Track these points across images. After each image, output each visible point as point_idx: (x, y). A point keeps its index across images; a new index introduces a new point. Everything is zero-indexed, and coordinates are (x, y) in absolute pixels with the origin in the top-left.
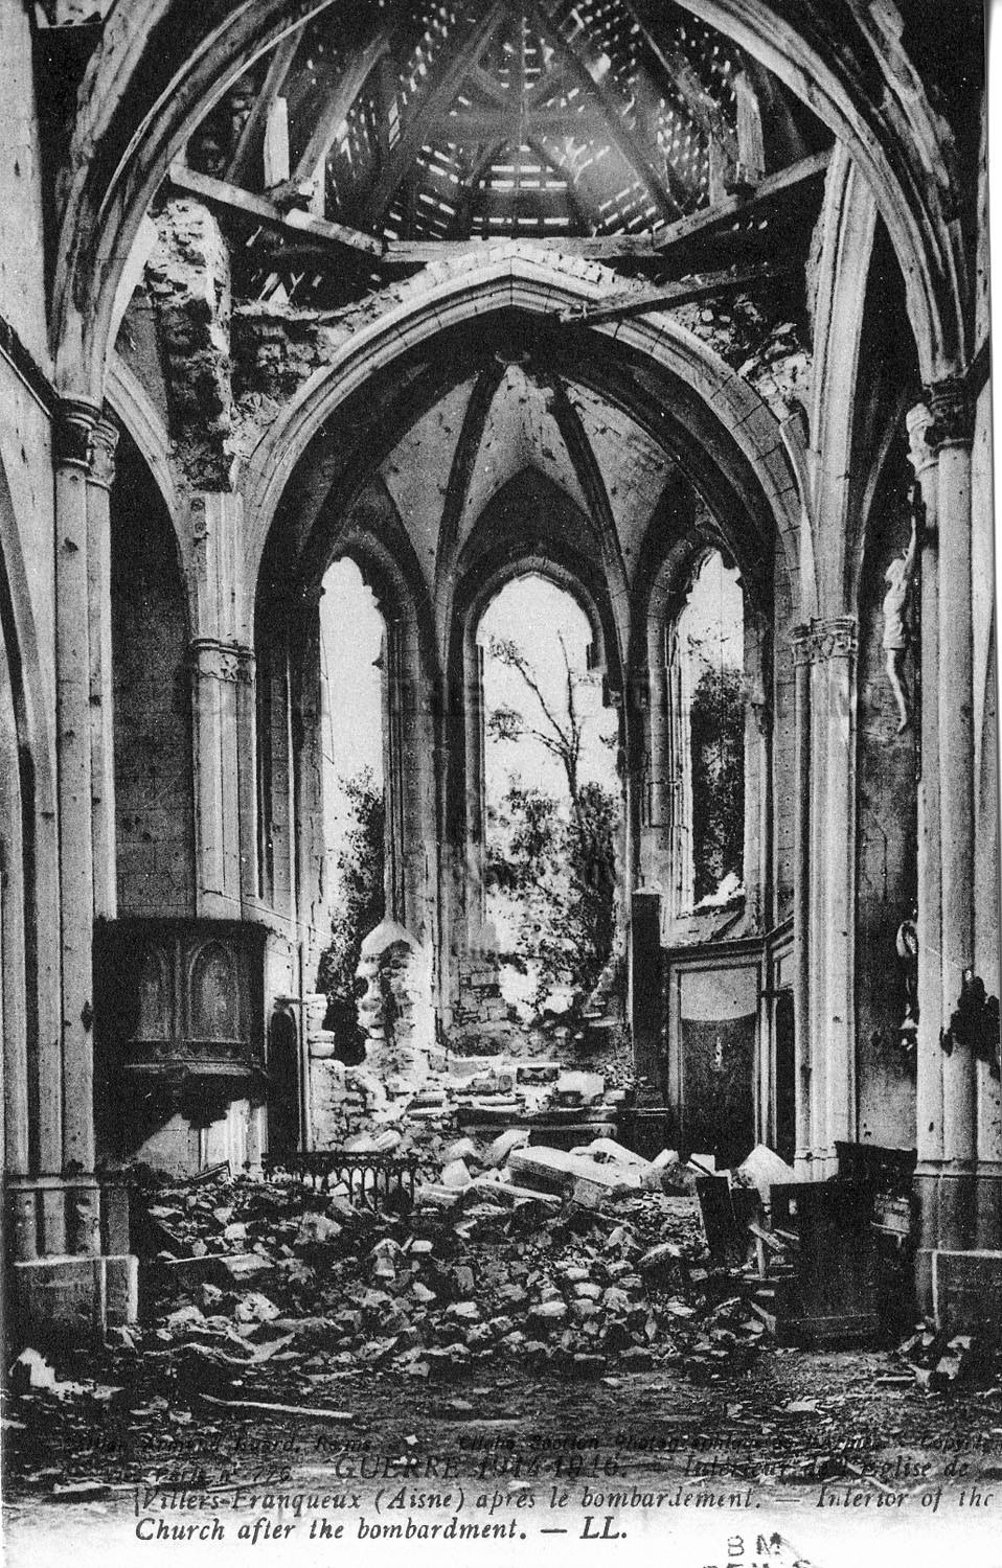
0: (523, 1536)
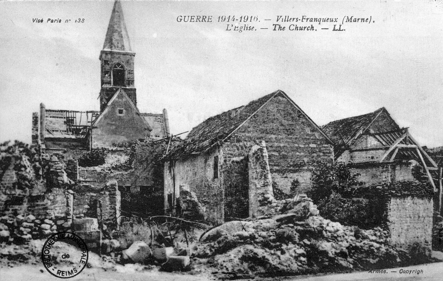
0: (374, 22)
